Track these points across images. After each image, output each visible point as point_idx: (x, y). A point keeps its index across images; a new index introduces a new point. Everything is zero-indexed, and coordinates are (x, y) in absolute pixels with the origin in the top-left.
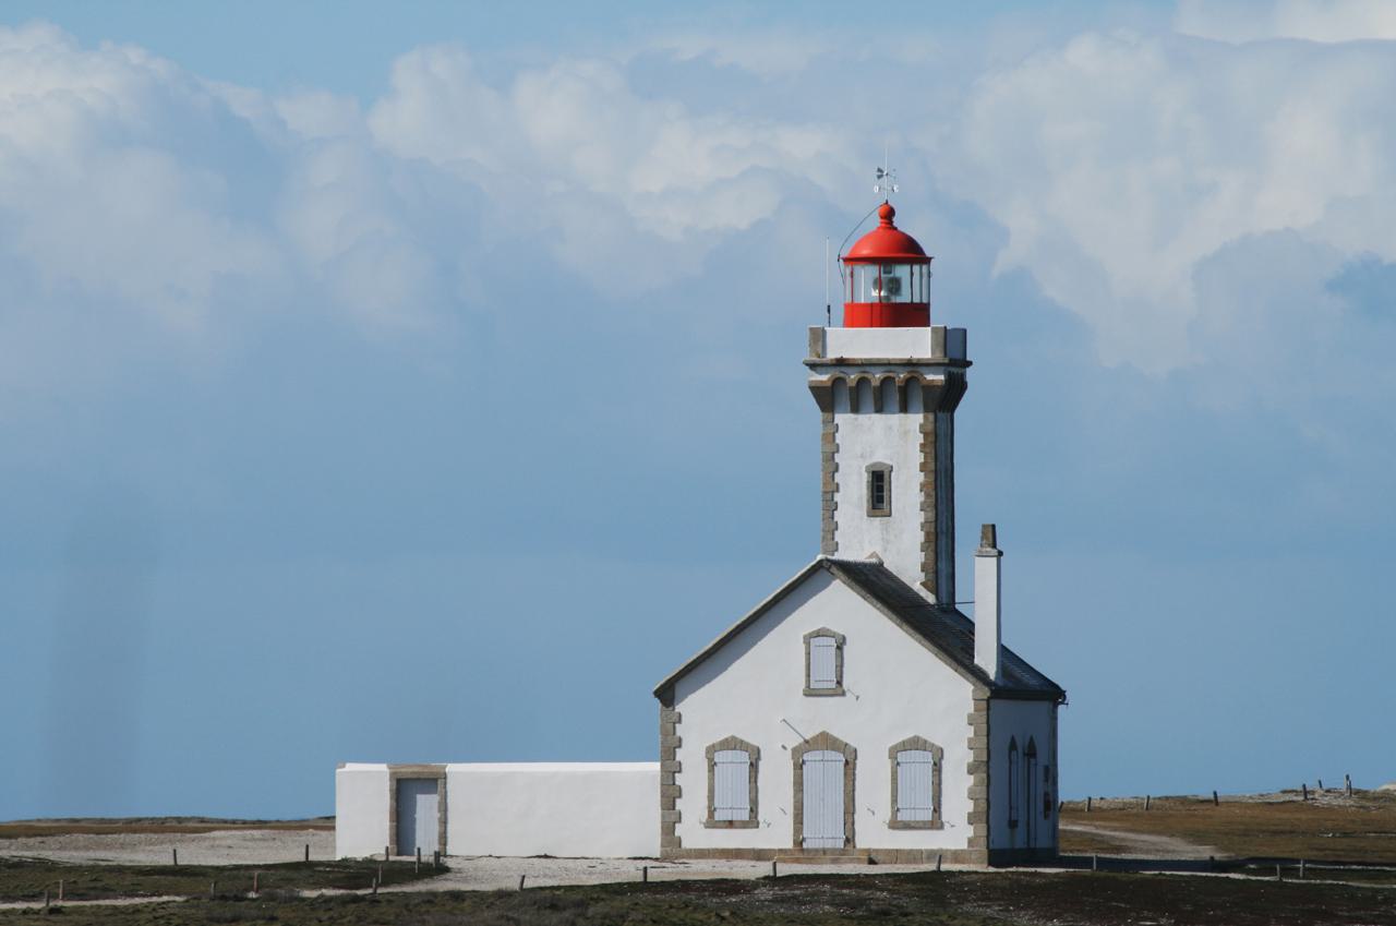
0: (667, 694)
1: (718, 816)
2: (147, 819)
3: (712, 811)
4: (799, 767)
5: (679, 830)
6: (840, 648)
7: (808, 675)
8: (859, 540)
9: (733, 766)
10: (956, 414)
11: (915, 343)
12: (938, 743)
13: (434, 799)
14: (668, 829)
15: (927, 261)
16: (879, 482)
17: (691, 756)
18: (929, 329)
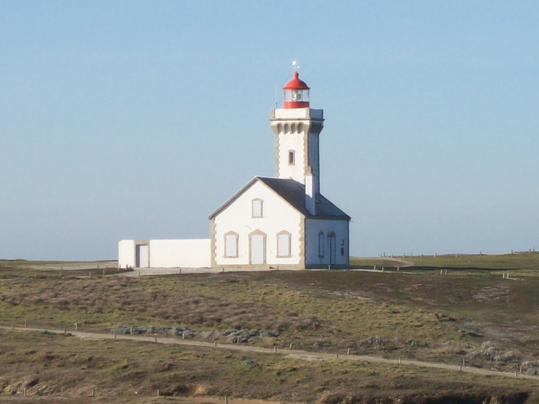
0: (213, 217)
1: (227, 255)
2: (258, 265)
3: (225, 253)
4: (250, 240)
5: (216, 259)
6: (262, 203)
7: (253, 212)
8: (285, 172)
9: (231, 239)
10: (321, 135)
11: (303, 113)
12: (290, 232)
13: (146, 247)
14: (213, 259)
15: (308, 89)
16: (291, 155)
17: (219, 237)
18: (308, 108)
